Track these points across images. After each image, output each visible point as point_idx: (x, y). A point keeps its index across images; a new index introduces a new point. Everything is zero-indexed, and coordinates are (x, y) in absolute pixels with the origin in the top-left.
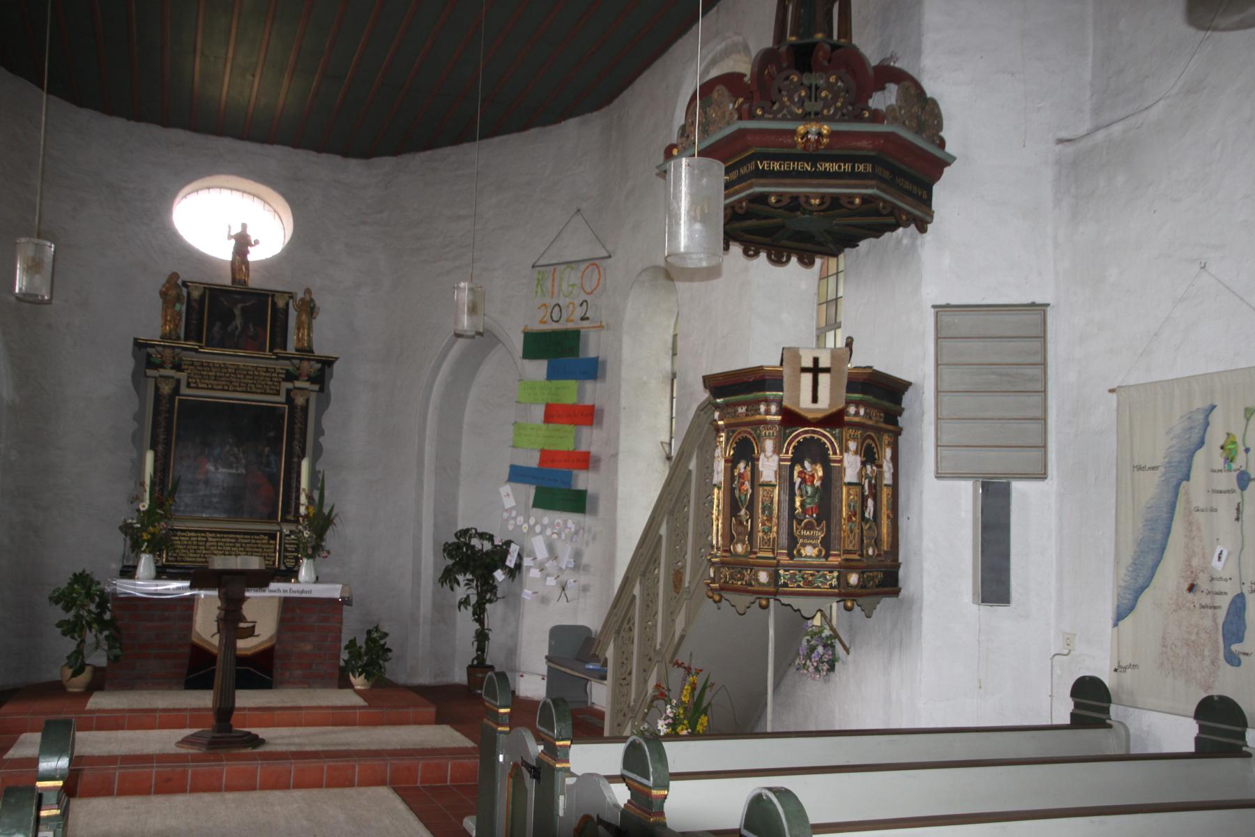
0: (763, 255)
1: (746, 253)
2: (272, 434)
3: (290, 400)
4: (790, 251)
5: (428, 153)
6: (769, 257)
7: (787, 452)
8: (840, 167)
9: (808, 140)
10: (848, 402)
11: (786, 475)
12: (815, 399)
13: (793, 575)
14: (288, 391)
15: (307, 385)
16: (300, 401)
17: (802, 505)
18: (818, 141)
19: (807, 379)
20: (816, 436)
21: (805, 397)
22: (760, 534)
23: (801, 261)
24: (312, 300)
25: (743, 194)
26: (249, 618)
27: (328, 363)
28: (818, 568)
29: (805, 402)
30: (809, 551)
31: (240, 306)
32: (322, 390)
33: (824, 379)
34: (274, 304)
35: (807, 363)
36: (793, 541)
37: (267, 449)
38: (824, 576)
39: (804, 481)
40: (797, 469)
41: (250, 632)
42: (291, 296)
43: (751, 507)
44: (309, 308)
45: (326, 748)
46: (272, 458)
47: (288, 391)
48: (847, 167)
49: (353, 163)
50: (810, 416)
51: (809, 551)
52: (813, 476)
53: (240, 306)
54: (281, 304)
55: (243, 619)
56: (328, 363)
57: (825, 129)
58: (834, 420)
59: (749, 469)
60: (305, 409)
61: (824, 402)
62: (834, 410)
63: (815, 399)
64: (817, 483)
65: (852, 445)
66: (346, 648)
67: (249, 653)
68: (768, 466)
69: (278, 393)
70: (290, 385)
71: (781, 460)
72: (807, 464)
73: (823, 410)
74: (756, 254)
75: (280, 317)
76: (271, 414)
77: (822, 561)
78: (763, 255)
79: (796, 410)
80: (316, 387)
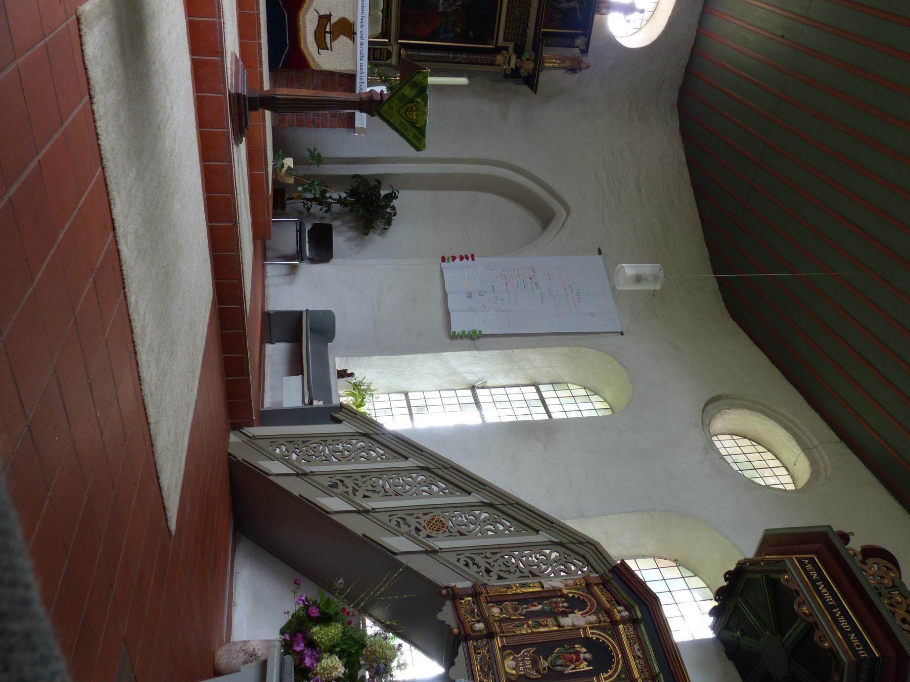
2: (471, 34)
3: (498, 50)
7: (592, 633)
14: (506, 49)
15: (512, 65)
16: (499, 59)
20: (610, 672)
24: (581, 69)
25: (801, 586)
26: (335, 43)
27: (531, 82)
30: (509, 663)
31: (577, 6)
32: (506, 76)
34: (577, 36)
36: (516, 649)
37: (459, 30)
41: (322, 45)
42: (585, 51)
44: (575, 68)
46: (451, 35)
47: (506, 49)
49: (676, 95)
51: (509, 663)
53: (577, 6)
54: (578, 41)
55: (333, 39)
56: (531, 82)
59: (584, 667)
60: (492, 64)
66: (657, 675)
67: (302, 46)
68: (575, 619)
69: (505, 39)
70: (511, 50)
71: (584, 629)
75: (567, 41)
76: (489, 33)
80: (508, 72)
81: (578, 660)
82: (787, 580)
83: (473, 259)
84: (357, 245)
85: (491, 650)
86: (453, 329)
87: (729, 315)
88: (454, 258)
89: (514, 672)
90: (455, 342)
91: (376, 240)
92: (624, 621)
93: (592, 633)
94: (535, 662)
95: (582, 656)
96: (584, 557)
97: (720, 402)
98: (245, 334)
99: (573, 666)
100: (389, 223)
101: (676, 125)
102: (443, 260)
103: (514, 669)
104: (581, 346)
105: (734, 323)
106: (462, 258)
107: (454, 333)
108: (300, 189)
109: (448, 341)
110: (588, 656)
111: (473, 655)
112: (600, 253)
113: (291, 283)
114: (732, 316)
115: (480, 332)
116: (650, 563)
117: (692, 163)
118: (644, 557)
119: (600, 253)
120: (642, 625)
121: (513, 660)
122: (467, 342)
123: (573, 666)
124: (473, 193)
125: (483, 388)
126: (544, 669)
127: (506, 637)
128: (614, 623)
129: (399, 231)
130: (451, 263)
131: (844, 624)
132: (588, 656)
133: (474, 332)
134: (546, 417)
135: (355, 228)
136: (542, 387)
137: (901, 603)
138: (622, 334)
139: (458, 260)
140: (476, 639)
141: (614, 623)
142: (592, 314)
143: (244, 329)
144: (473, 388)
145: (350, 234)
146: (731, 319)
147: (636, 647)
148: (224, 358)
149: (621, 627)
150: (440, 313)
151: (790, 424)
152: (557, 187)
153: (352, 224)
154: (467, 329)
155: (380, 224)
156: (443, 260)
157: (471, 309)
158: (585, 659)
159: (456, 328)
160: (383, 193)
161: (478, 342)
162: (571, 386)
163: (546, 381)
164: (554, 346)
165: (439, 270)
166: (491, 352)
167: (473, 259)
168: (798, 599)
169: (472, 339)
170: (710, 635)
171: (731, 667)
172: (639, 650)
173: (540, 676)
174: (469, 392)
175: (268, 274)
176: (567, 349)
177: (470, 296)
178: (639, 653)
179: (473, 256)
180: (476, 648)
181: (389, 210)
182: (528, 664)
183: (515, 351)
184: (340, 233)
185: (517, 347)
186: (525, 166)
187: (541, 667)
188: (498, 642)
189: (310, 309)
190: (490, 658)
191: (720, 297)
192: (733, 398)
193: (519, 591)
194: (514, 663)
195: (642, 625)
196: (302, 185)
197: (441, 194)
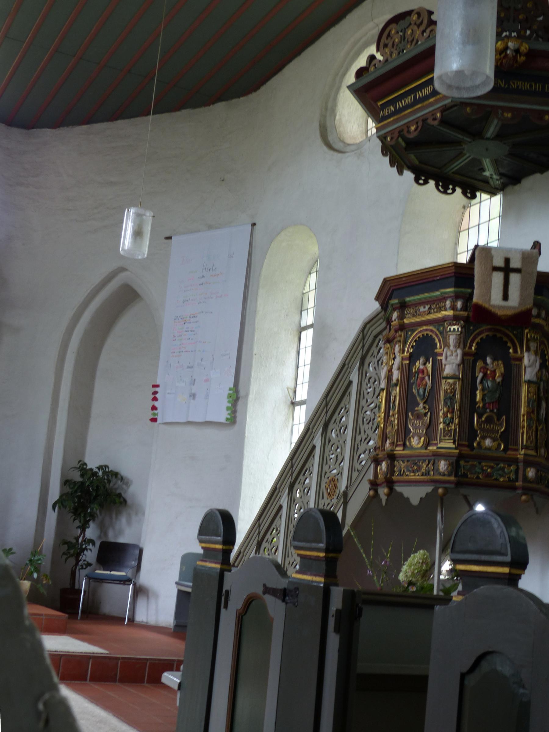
0: (432, 183)
1: (417, 180)
4: (456, 184)
5: (85, 127)
6: (437, 186)
8: (531, 86)
9: (506, 55)
10: (536, 304)
11: (469, 362)
12: (505, 297)
13: (473, 466)
17: (483, 399)
18: (515, 58)
19: (498, 278)
21: (492, 295)
22: (441, 426)
23: (464, 193)
28: (497, 460)
29: (495, 299)
33: (515, 278)
35: (499, 262)
38: (503, 469)
39: (485, 376)
40: (479, 364)
43: (430, 399)
45: (106, 683)
48: (538, 87)
49: (15, 131)
50: (500, 313)
52: (494, 372)
57: (524, 48)
58: (520, 320)
59: (429, 366)
61: (515, 299)
62: (523, 309)
63: (505, 297)
64: (498, 379)
65: (533, 346)
72: (489, 360)
73: (514, 308)
74: (426, 182)
77: (502, 454)
78: (432, 183)
79: (486, 305)
81: (423, 372)
82: (392, 139)
83: (158, 386)
84: (136, 514)
85: (402, 457)
86: (223, 420)
87: (254, 94)
88: (154, 408)
89: (422, 439)
90: (238, 419)
91: (132, 491)
92: (401, 317)
93: (407, 352)
94: (418, 417)
95: (422, 367)
96: (376, 337)
97: (328, 124)
98: (123, 658)
99: (427, 378)
100: (116, 474)
101: (47, 133)
102: (154, 420)
103: (421, 438)
104: (260, 274)
105: (263, 88)
106: (155, 399)
107: (227, 419)
108: (35, 575)
109: (236, 427)
110: (422, 360)
111: (405, 478)
112: (170, 238)
113: (156, 596)
114: (255, 90)
115: (230, 389)
116: (463, 236)
117: (89, 120)
118: (456, 244)
119: (170, 238)
120: (408, 299)
121: (413, 438)
122: (240, 403)
123: (427, 378)
124: (98, 373)
125: (295, 392)
126: (424, 408)
127: (397, 442)
128: (402, 327)
129: (125, 463)
130: (159, 411)
131: (409, 100)
132: (422, 360)
133: (230, 396)
134: (311, 331)
135: (119, 513)
136: (303, 324)
137: (412, 31)
138: (254, 225)
139: (156, 404)
140: (393, 473)
141: (402, 327)
142: (230, 257)
143: (147, 659)
144: (294, 404)
145: (123, 520)
146: (258, 92)
147: (422, 309)
148: (148, 682)
149: (406, 321)
150: (210, 432)
151: (356, 48)
152: (97, 279)
153: (114, 516)
154: (225, 403)
155: (115, 484)
156: (154, 420)
157: (207, 397)
158: (425, 364)
159: (222, 416)
160: (78, 479)
161: (242, 393)
162: (306, 290)
163: (298, 318)
164: (256, 307)
165: (164, 426)
166: (252, 380)
167: (158, 386)
168: (430, 121)
169: (236, 398)
170: (497, 199)
171: (527, 182)
172: (424, 307)
173: (429, 414)
174: (297, 408)
175: (145, 620)
176: (261, 292)
177: (193, 396)
178: (427, 307)
179: (154, 386)
180: (400, 475)
181: (100, 473)
182: (418, 423)
183: (255, 351)
184: (121, 532)
185: (251, 349)
186: (70, 314)
187: (423, 411)
188: (399, 450)
189: (177, 579)
190: (408, 461)
191: (234, 101)
192: (326, 109)
193: (383, 415)
194: (416, 438)
195: (408, 299)
196: (32, 573)
197: (96, 410)
